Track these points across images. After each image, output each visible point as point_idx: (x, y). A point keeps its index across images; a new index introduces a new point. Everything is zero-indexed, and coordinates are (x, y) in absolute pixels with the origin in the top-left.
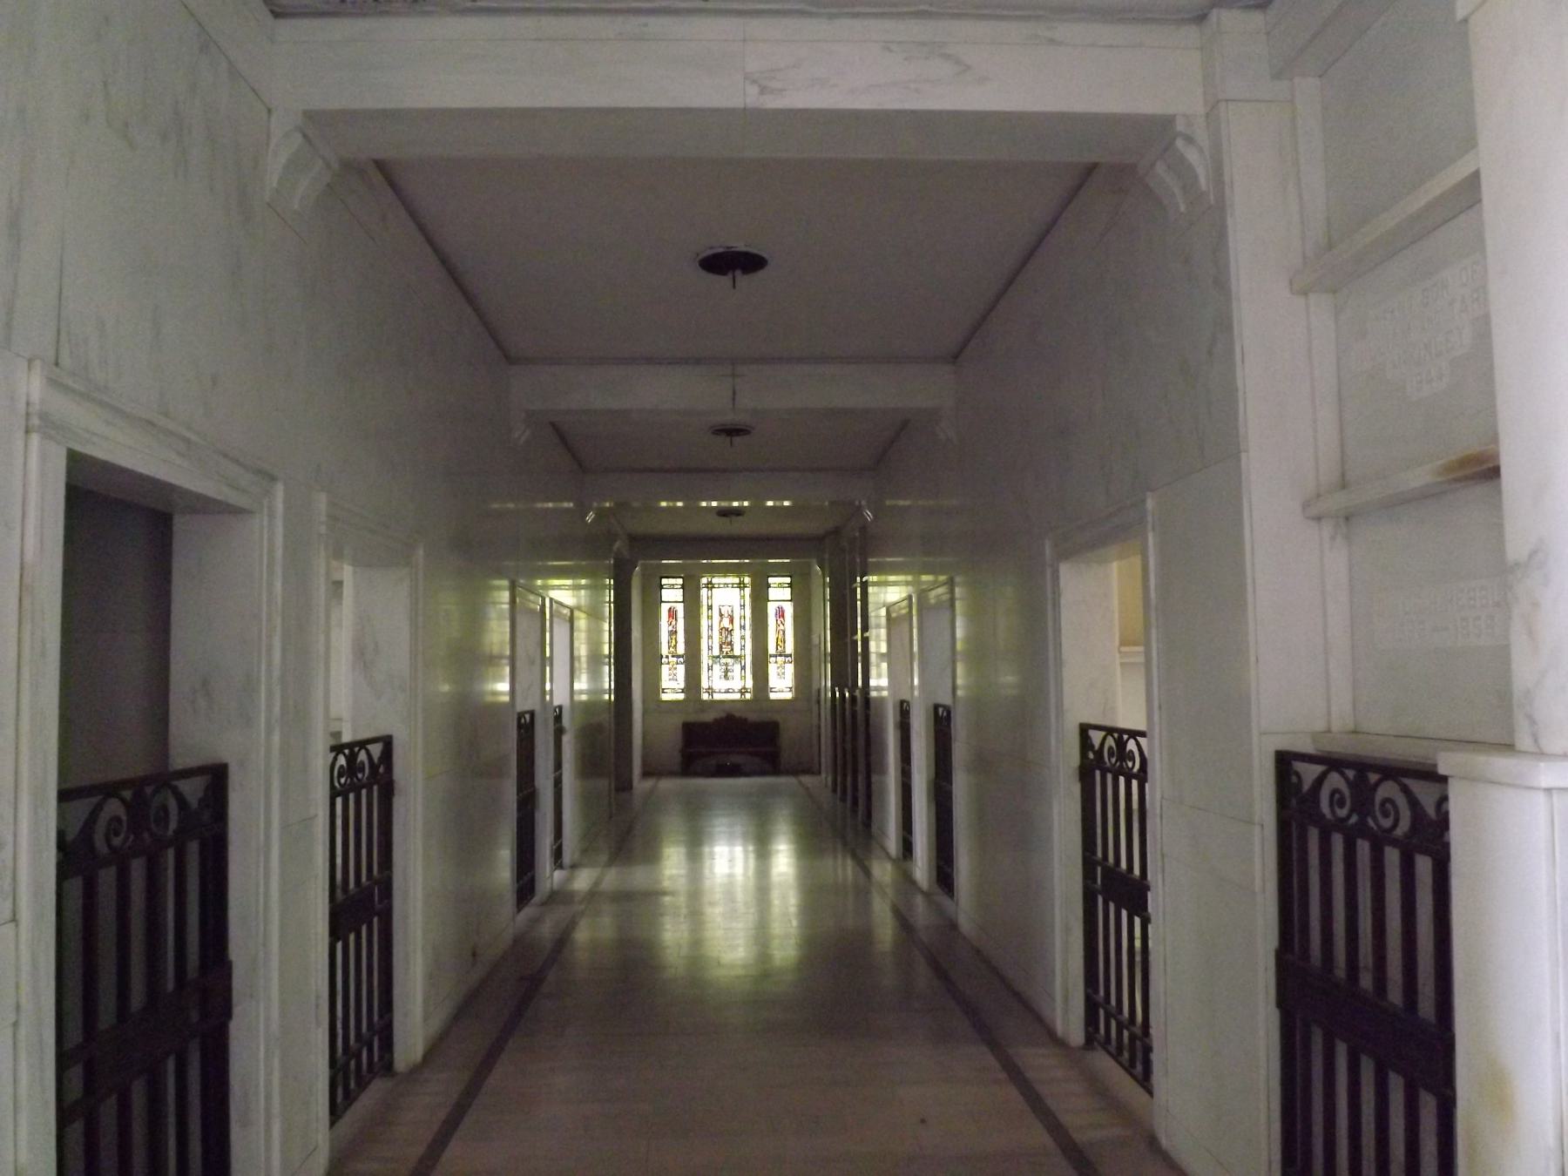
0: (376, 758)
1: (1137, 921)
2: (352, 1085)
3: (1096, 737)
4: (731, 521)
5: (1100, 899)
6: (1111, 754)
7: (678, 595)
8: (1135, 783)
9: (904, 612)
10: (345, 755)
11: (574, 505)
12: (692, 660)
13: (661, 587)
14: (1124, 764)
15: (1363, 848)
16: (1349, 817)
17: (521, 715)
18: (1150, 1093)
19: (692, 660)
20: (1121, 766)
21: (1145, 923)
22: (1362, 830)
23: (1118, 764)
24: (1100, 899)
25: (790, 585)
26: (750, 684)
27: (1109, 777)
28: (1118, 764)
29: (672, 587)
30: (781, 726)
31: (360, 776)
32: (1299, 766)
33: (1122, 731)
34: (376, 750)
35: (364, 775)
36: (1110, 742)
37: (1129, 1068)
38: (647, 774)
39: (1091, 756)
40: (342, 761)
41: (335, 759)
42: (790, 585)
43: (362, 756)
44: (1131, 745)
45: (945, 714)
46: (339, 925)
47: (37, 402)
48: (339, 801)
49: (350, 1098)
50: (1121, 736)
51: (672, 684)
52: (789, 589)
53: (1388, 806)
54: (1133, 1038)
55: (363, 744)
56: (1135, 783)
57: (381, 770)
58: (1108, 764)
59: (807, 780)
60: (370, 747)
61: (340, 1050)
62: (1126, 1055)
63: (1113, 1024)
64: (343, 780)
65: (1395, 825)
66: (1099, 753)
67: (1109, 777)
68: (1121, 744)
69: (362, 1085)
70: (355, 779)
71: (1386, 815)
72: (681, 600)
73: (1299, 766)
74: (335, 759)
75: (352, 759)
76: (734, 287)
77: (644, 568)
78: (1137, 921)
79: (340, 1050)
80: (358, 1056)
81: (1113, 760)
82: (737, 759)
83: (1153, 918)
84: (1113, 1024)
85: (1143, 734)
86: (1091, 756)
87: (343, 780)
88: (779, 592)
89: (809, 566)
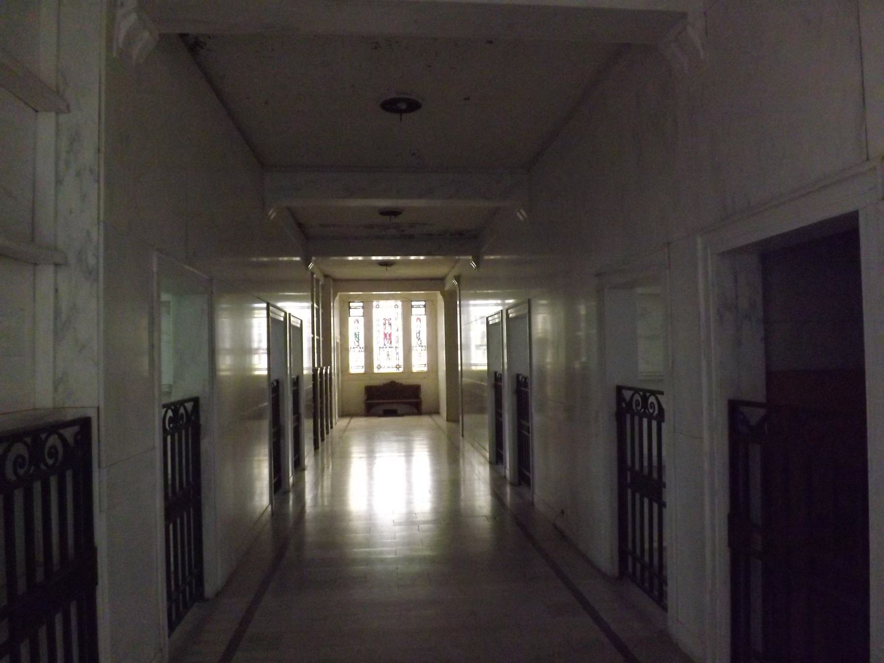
0: (70, 439)
1: (655, 506)
2: (181, 608)
3: (627, 394)
4: (386, 269)
5: (629, 491)
6: (637, 405)
7: (360, 312)
8: (654, 424)
9: (497, 321)
10: (171, 409)
11: (301, 258)
12: (368, 350)
13: (350, 308)
14: (647, 411)
15: (645, 421)
16: (641, 410)
17: (175, 406)
18: (665, 608)
19: (368, 350)
20: (644, 411)
21: (662, 505)
22: (644, 415)
23: (643, 410)
24: (629, 491)
25: (425, 306)
26: (401, 363)
27: (636, 418)
28: (643, 410)
29: (419, 307)
30: (422, 386)
31: (181, 422)
32: (745, 410)
33: (645, 391)
34: (189, 406)
35: (183, 421)
36: (637, 397)
37: (649, 592)
38: (343, 414)
39: (624, 405)
40: (170, 414)
41: (166, 412)
42: (425, 306)
43: (182, 411)
44: (652, 399)
45: (523, 380)
46: (170, 514)
47: (477, 467)
48: (169, 438)
49: (180, 618)
50: (645, 393)
51: (356, 364)
52: (424, 308)
53: (652, 405)
54: (643, 567)
55: (182, 403)
56: (654, 424)
57: (193, 418)
58: (635, 411)
59: (435, 417)
60: (187, 405)
61: (173, 588)
62: (647, 585)
63: (638, 565)
64: (171, 425)
65: (654, 413)
66: (629, 404)
67: (636, 418)
68: (645, 399)
69: (187, 608)
70: (43, 467)
71: (651, 408)
72: (362, 315)
73: (745, 410)
74: (166, 412)
75: (175, 412)
76: (401, 120)
77: (340, 297)
78: (655, 506)
79: (173, 588)
80: (184, 591)
81: (639, 408)
82: (394, 407)
83: (668, 504)
84: (638, 565)
85: (662, 393)
86: (624, 405)
87: (171, 425)
88: (419, 311)
89: (436, 296)
